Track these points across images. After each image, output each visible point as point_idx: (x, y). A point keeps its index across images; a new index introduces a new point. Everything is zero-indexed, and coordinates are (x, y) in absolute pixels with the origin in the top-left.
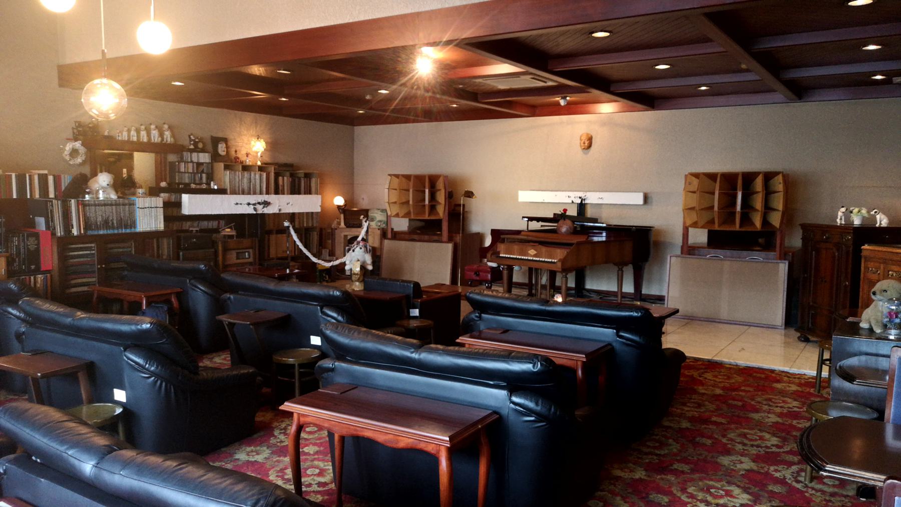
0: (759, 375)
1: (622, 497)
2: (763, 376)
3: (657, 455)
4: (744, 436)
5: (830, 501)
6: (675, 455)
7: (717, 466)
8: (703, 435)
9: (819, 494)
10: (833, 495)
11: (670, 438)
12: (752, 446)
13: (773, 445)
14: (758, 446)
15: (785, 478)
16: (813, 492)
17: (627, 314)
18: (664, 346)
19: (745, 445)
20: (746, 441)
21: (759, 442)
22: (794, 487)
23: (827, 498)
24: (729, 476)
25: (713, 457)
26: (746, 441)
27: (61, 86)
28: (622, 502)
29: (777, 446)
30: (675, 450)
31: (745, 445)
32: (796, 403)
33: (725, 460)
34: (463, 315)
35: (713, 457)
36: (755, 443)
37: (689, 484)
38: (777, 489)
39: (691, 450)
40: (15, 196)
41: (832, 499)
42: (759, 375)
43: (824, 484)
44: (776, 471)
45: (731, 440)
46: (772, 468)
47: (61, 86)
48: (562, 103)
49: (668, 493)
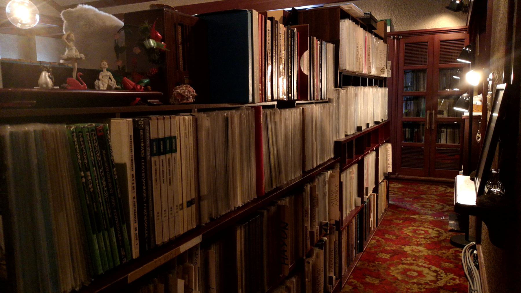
0: (412, 191)
2: (409, 191)
5: (414, 260)
6: (391, 265)
9: (420, 264)
10: (411, 264)
11: (402, 281)
15: (446, 273)
16: (424, 265)
17: (155, 147)
18: (474, 204)
22: (437, 267)
23: (415, 262)
25: (364, 265)
27: (173, 150)
30: (392, 268)
35: (364, 265)
38: (447, 265)
40: (454, 77)
41: (412, 262)
42: (412, 191)
43: (417, 271)
44: (454, 279)
46: (458, 281)
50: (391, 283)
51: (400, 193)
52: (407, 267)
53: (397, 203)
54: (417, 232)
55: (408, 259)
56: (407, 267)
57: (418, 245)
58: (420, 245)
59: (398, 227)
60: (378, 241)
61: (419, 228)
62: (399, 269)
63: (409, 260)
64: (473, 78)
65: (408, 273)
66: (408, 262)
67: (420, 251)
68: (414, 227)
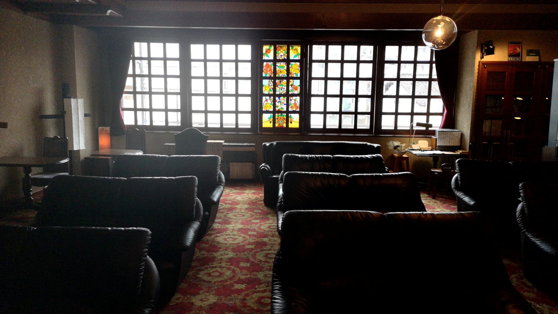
1: (254, 310)
2: (255, 211)
3: (258, 292)
4: (234, 239)
7: (249, 204)
8: (254, 235)
10: (270, 250)
12: (229, 235)
13: (203, 270)
14: (227, 235)
19: (233, 235)
20: (232, 236)
21: (226, 237)
24: (244, 203)
26: (232, 236)
27: (6, 127)
28: (252, 306)
29: (217, 236)
31: (233, 235)
32: (238, 198)
33: (246, 206)
34: (425, 200)
36: (228, 236)
37: (231, 275)
39: (238, 303)
45: (240, 236)
47: (6, 127)
48: (478, 59)
49: (250, 236)
50: (258, 264)
51: (248, 215)
52: (267, 252)
53: (247, 227)
54: (269, 256)
55: (267, 246)
56: (260, 295)
57: (273, 236)
58: (275, 236)
59: (251, 253)
60: (244, 237)
61: (269, 252)
62: (253, 298)
63: (268, 247)
64: (147, 312)
65: (269, 256)
66: (262, 289)
67: (275, 241)
68: (265, 252)
